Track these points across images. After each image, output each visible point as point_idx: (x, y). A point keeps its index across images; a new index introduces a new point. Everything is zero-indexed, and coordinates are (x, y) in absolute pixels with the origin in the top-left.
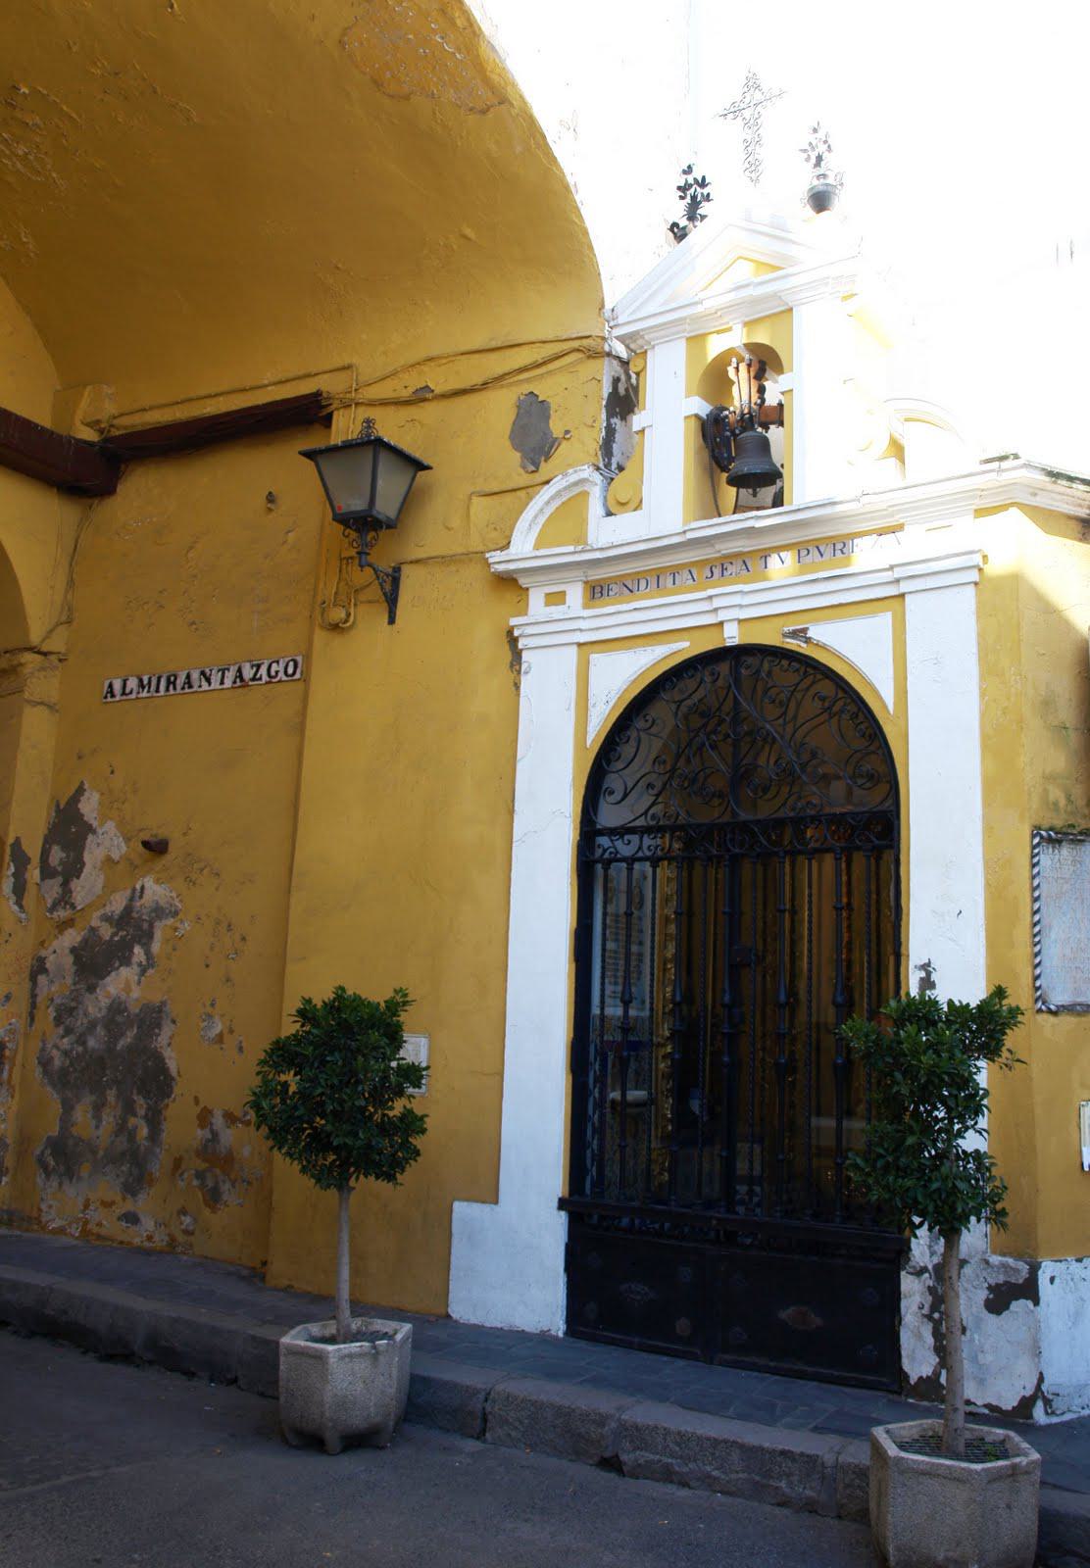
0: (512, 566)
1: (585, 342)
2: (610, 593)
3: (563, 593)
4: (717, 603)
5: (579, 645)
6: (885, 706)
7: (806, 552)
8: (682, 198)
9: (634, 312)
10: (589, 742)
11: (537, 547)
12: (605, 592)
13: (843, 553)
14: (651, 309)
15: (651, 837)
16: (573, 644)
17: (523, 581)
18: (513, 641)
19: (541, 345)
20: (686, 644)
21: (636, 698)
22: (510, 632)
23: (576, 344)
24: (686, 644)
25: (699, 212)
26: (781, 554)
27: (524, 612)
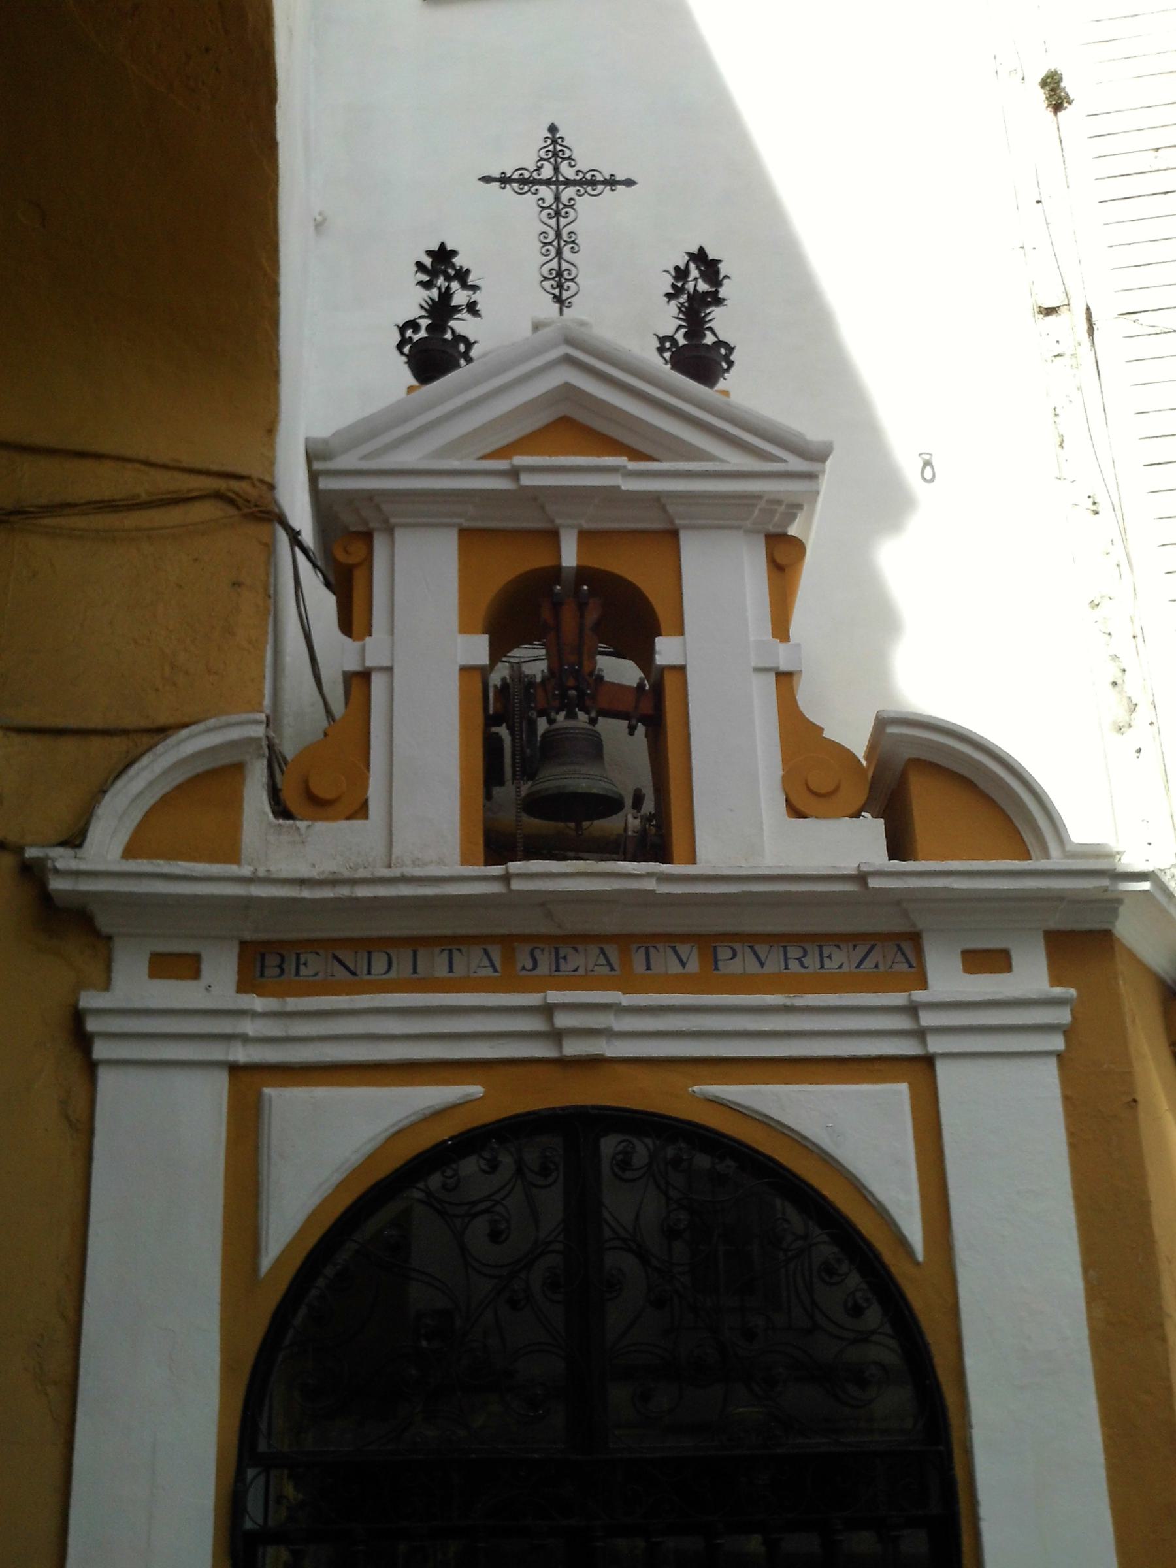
0: (86, 886)
1: (235, 485)
2: (303, 969)
3: (196, 958)
4: (535, 1024)
5: (234, 1069)
6: (902, 1242)
7: (729, 954)
8: (426, 285)
9: (364, 457)
10: (266, 1263)
11: (129, 852)
12: (290, 966)
13: (803, 966)
14: (408, 457)
16: (392, 660)
17: (103, 923)
18: (82, 1040)
19: (143, 468)
20: (477, 1090)
22: (78, 1017)
23: (221, 485)
24: (477, 1090)
25: (452, 323)
26: (757, 948)
27: (107, 986)
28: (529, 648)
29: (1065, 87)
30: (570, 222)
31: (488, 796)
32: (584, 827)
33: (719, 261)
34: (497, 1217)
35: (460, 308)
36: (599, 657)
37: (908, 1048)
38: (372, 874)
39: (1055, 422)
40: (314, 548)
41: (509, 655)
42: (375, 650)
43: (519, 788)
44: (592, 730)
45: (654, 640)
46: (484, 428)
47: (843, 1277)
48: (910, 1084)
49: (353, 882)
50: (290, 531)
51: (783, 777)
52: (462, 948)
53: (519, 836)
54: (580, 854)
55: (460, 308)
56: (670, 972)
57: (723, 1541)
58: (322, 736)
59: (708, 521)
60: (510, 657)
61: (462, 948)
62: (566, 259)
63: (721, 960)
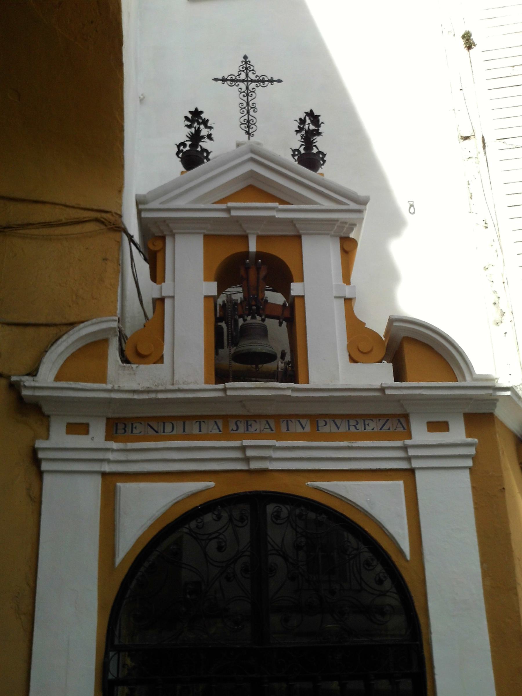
0: (38, 393)
1: (104, 215)
2: (134, 430)
3: (87, 425)
4: (237, 455)
5: (104, 475)
6: (401, 551)
8: (189, 127)
10: (118, 561)
11: (57, 378)
13: (356, 429)
15: (322, 162)
16: (174, 293)
17: (46, 410)
18: (37, 462)
19: (63, 208)
20: (212, 484)
21: (155, 537)
22: (35, 451)
23: (98, 215)
24: (212, 484)
25: (201, 144)
27: (47, 438)
28: (235, 288)
29: (473, 39)
30: (253, 98)
31: (217, 353)
32: (259, 367)
33: (319, 116)
34: (221, 540)
35: (204, 137)
36: (266, 292)
37: (403, 465)
38: (165, 388)
39: (468, 187)
40: (139, 243)
41: (226, 291)
42: (166, 289)
43: (230, 350)
44: (263, 324)
45: (290, 284)
46: (215, 190)
47: (374, 567)
48: (404, 481)
49: (157, 391)
50: (129, 236)
51: (348, 345)
52: (205, 421)
53: (230, 371)
54: (258, 379)
55: (204, 137)
56: (297, 432)
57: (321, 684)
58: (143, 327)
59: (314, 231)
60: (226, 291)
61: (205, 421)
62: (251, 115)
63: (320, 426)
